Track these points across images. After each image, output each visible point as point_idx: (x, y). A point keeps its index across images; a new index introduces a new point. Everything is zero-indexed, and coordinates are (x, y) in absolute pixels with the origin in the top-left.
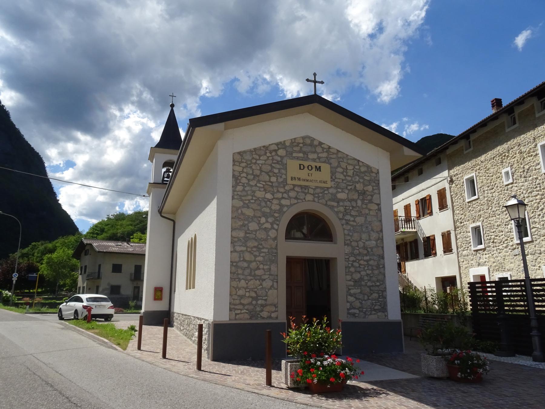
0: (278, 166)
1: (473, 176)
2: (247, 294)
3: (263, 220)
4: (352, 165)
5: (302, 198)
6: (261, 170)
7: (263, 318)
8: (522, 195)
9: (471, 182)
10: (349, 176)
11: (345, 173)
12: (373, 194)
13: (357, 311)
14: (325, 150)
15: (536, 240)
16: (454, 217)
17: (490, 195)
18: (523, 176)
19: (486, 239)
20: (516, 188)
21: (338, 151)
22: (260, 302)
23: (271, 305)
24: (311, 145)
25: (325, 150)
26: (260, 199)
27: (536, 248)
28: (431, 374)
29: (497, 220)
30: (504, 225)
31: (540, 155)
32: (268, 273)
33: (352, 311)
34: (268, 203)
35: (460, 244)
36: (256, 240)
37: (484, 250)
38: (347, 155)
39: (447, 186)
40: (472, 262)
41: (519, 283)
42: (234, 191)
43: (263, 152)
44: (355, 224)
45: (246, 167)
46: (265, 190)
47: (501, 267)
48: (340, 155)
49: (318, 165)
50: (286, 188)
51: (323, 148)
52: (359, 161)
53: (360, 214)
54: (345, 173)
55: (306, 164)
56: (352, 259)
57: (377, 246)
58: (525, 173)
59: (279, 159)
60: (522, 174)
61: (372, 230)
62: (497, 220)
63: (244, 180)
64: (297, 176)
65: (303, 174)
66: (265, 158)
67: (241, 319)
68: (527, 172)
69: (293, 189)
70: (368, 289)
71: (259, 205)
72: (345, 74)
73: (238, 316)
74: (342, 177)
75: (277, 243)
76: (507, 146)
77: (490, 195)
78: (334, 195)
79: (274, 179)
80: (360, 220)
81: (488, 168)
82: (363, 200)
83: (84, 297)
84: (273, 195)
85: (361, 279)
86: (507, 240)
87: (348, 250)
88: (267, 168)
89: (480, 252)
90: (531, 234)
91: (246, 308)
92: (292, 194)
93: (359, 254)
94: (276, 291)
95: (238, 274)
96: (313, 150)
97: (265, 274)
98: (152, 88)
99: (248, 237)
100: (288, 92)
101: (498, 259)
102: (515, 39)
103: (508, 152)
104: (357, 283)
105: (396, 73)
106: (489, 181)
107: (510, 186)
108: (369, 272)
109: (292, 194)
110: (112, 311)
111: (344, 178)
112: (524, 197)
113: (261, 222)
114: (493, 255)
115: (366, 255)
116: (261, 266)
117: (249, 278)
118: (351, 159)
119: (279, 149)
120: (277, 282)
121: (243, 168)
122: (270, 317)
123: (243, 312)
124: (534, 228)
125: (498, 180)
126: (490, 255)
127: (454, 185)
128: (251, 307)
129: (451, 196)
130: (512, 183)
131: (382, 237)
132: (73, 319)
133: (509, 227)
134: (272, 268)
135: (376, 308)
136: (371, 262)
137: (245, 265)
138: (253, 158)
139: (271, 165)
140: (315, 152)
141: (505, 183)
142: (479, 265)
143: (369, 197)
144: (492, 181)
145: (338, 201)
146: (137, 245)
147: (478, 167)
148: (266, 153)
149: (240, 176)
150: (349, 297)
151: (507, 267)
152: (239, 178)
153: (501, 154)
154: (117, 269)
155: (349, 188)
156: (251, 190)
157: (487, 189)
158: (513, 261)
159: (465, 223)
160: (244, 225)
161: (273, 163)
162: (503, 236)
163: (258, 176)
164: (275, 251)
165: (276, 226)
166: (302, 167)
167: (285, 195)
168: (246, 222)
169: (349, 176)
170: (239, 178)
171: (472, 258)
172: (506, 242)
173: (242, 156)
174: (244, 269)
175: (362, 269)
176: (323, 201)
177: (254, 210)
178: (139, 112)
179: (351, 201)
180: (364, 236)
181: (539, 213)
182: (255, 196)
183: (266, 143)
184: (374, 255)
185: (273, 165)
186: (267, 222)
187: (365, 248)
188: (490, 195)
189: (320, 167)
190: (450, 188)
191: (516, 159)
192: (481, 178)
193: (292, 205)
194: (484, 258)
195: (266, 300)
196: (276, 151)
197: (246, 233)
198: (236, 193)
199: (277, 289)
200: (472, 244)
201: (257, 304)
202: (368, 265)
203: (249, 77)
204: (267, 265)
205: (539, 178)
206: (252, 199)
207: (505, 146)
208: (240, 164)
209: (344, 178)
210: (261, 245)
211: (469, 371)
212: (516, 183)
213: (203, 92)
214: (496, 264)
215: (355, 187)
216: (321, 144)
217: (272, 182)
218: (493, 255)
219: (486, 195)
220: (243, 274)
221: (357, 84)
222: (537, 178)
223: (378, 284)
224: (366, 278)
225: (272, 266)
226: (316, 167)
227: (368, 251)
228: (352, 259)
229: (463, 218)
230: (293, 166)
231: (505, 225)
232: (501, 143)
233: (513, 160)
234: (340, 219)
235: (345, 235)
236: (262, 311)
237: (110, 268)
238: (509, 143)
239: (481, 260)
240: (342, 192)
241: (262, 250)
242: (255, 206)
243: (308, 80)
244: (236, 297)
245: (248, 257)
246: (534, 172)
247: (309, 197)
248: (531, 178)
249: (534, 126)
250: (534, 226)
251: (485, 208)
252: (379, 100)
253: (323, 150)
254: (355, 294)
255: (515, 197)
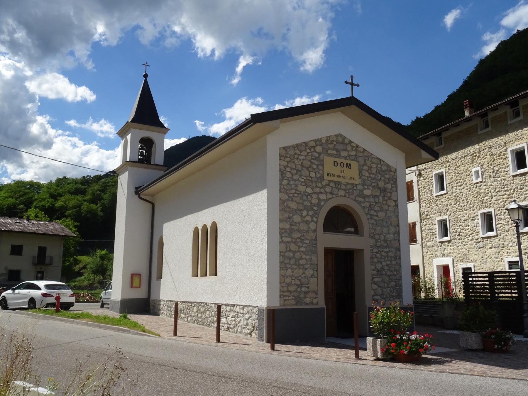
0: (316, 162)
1: (443, 172)
2: (293, 282)
3: (305, 213)
4: (375, 163)
5: (336, 193)
6: (302, 165)
7: (306, 304)
8: (490, 194)
9: (440, 178)
10: (373, 174)
11: (370, 171)
12: (391, 191)
13: (379, 298)
14: (354, 149)
15: (500, 235)
16: (420, 209)
17: (459, 191)
18: (492, 176)
19: (452, 231)
20: (485, 187)
21: (364, 150)
22: (303, 289)
23: (312, 292)
24: (343, 143)
25: (354, 149)
26: (302, 193)
27: (500, 242)
28: (469, 347)
29: (464, 215)
30: (470, 220)
31: (510, 159)
32: (310, 262)
33: (376, 297)
34: (309, 197)
35: (425, 235)
36: (299, 232)
37: (449, 242)
38: (372, 154)
39: (415, 179)
40: (436, 253)
41: (507, 274)
42: (281, 185)
43: (304, 149)
44: (377, 218)
45: (290, 161)
46: (306, 185)
47: (465, 258)
48: (366, 154)
49: (349, 162)
50: (323, 183)
51: (353, 147)
52: (380, 160)
53: (382, 210)
54: (370, 171)
55: (339, 161)
56: (375, 250)
57: (394, 239)
58: (494, 174)
59: (317, 155)
60: (491, 174)
61: (391, 225)
62: (464, 215)
63: (289, 175)
64: (332, 172)
65: (337, 171)
66: (305, 153)
67: (288, 305)
68: (496, 173)
69: (329, 185)
70: (387, 278)
71: (301, 198)
72: (267, 36)
73: (286, 302)
74: (367, 174)
75: (316, 234)
76: (478, 147)
77: (459, 191)
78: (361, 191)
79: (313, 174)
80: (382, 215)
81: (458, 165)
82: (384, 197)
83: (41, 283)
84: (313, 190)
85: (382, 269)
86: (473, 233)
87: (372, 242)
88: (307, 163)
89: (446, 243)
90: (496, 229)
91: (292, 294)
92: (328, 189)
93: (380, 247)
94: (316, 279)
95: (285, 264)
96: (344, 148)
97: (307, 264)
98: (29, 28)
99: (292, 229)
100: (200, 49)
101: (463, 250)
102: (444, 18)
103: (480, 153)
104: (379, 272)
105: (323, 37)
106: (458, 178)
107: (479, 184)
108: (388, 262)
109: (328, 189)
110: (73, 300)
111: (369, 175)
112: (492, 196)
113: (303, 215)
114: (458, 247)
115: (386, 247)
116: (304, 256)
117: (295, 267)
118: (375, 158)
119: (317, 145)
120: (317, 271)
121: (288, 162)
122: (312, 303)
123: (290, 298)
124: (499, 224)
125: (468, 178)
126: (455, 246)
127: (422, 178)
128: (296, 294)
129: (419, 189)
130: (481, 182)
131: (399, 231)
132: (26, 309)
133: (476, 221)
134: (313, 259)
135: (394, 294)
136: (390, 254)
137: (291, 255)
138: (296, 154)
139: (310, 161)
140: (345, 150)
141: (475, 181)
142: (443, 255)
143: (389, 195)
144: (462, 178)
145: (365, 197)
146: (39, 222)
147: (448, 164)
148: (306, 149)
149: (285, 170)
150: (373, 285)
151: (471, 259)
152: (285, 172)
153: (473, 154)
154: (17, 250)
155: (373, 185)
156: (295, 184)
157: (456, 185)
158: (477, 253)
159: (431, 216)
160: (289, 218)
161: (312, 159)
162: (469, 230)
163: (300, 171)
164: (315, 242)
165: (315, 219)
166: (336, 165)
167: (322, 190)
168: (291, 215)
169: (373, 174)
170: (285, 172)
171: (436, 249)
172: (472, 235)
173: (286, 151)
174: (290, 259)
175: (383, 260)
176: (353, 197)
177: (298, 203)
178: (10, 54)
179: (374, 197)
180: (385, 230)
181: (504, 211)
182: (298, 191)
183: (306, 140)
184: (392, 247)
185: (312, 161)
186: (308, 215)
187: (385, 241)
188: (459, 191)
189: (350, 164)
190: (418, 181)
191: (486, 160)
192: (450, 174)
193: (328, 200)
194: (449, 249)
195: (308, 287)
196: (314, 147)
197: (291, 225)
198: (282, 187)
199: (317, 277)
200: (437, 235)
201: (301, 291)
202: (388, 256)
203: (154, 25)
204: (308, 255)
205: (507, 179)
206: (296, 193)
207: (477, 147)
208: (285, 158)
209: (369, 175)
210: (303, 236)
211: (503, 343)
212: (485, 182)
213: (96, 37)
214: (494, 257)
215: (378, 184)
216: (350, 142)
217: (311, 178)
218: (458, 247)
219: (454, 191)
220: (290, 264)
221: (280, 48)
222: (505, 180)
223: (395, 273)
224: (386, 268)
225: (312, 256)
226: (347, 164)
227: (388, 244)
228: (375, 250)
229: (429, 211)
230: (328, 161)
231: (472, 220)
232: (473, 143)
233: (484, 161)
234: (366, 214)
235: (370, 228)
236: (305, 297)
237: (8, 249)
238: (481, 144)
239: (446, 251)
240: (368, 189)
241: (305, 241)
242: (297, 199)
243: (346, 82)
244: (284, 285)
245: (293, 247)
246: (503, 173)
247: (342, 193)
248: (499, 179)
249: (506, 132)
250: (499, 222)
251: (453, 203)
252: (302, 69)
253: (352, 149)
254: (377, 282)
255: (515, 201)
